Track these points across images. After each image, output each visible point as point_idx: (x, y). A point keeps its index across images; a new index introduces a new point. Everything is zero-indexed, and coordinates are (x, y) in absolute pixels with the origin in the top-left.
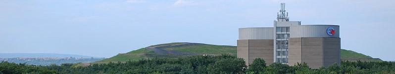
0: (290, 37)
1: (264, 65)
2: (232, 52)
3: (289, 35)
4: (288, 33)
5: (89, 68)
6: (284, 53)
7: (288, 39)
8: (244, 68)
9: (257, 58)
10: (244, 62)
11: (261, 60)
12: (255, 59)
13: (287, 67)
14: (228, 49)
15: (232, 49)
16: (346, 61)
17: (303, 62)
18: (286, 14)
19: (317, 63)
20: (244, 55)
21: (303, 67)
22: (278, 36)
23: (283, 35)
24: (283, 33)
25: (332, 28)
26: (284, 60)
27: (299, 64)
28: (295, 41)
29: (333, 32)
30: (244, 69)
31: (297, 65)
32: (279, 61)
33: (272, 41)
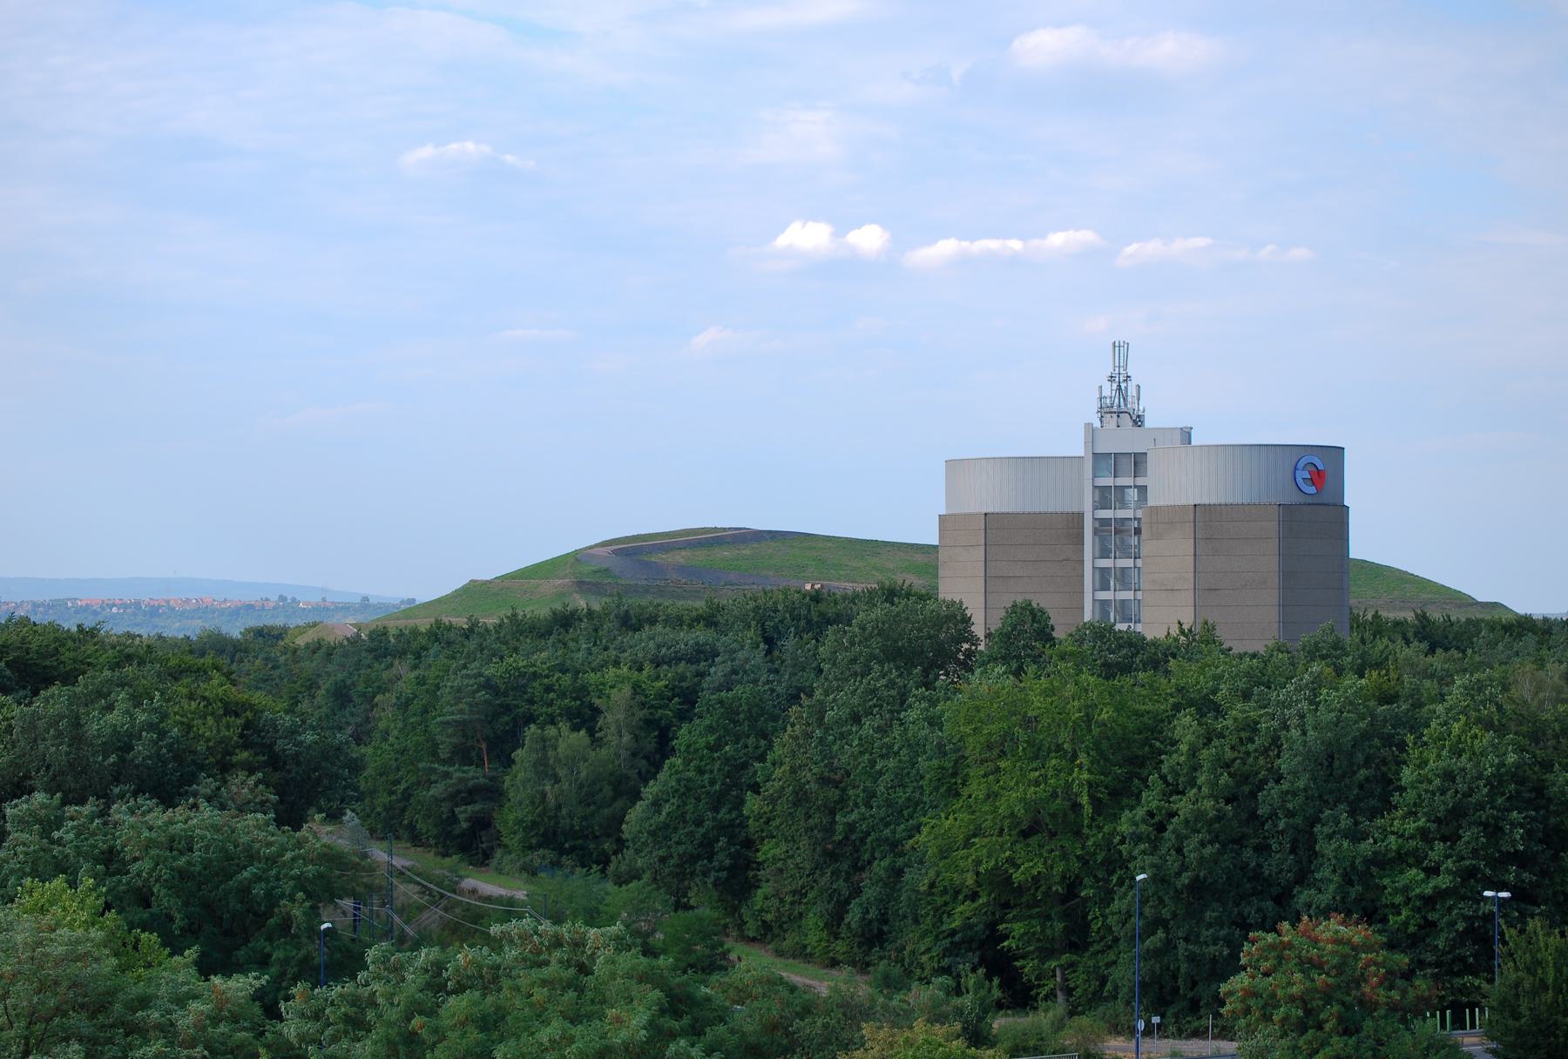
3: (1143, 490)
4: (1140, 481)
7: (1139, 514)
8: (966, 646)
9: (1019, 600)
10: (967, 621)
11: (1032, 611)
13: (1135, 644)
17: (1200, 620)
18: (1132, 391)
19: (1252, 628)
20: (963, 587)
21: (1199, 642)
22: (1105, 497)
24: (1121, 481)
28: (1168, 517)
29: (1317, 477)
30: (969, 654)
31: (1175, 631)
33: (1081, 516)
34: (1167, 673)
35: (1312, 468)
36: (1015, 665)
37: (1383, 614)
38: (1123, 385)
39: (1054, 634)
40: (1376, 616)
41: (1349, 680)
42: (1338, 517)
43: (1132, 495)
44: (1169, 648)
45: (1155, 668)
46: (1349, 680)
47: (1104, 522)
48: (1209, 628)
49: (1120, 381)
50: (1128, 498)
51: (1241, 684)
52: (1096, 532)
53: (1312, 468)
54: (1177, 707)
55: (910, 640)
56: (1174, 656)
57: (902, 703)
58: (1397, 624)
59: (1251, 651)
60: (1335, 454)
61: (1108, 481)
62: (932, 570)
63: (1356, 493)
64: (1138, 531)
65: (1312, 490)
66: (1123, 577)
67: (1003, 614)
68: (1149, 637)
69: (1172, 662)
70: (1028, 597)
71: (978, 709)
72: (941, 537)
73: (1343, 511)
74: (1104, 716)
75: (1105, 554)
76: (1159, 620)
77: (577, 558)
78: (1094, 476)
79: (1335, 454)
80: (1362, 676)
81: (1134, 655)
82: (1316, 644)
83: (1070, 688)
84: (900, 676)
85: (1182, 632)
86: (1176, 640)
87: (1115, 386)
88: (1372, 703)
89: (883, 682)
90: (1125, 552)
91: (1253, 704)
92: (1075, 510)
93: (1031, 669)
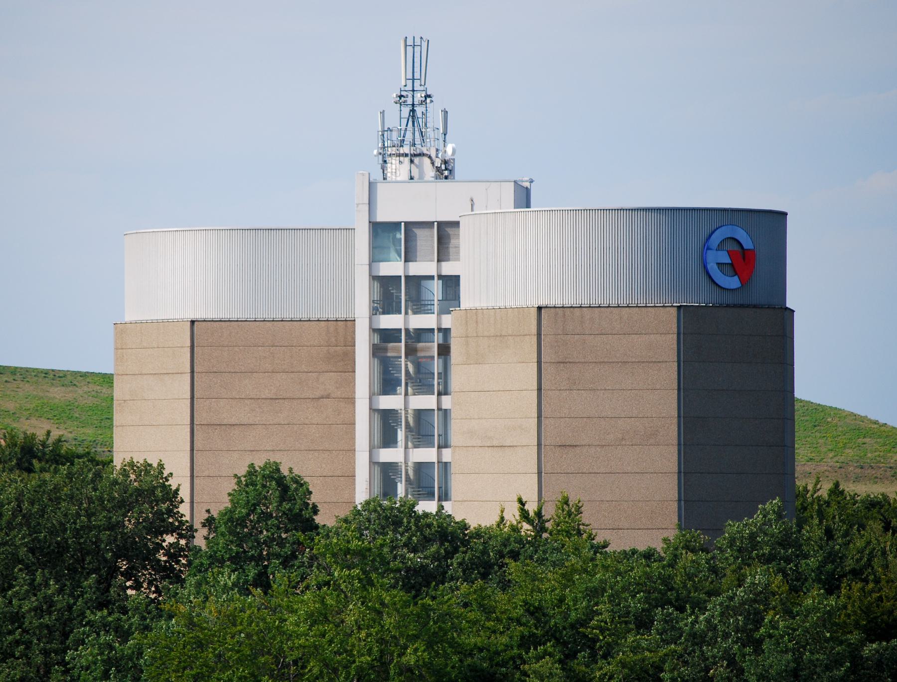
0: (467, 300)
1: (303, 520)
2: (63, 413)
3: (451, 283)
4: (448, 268)
5: (587, 552)
6: (422, 429)
7: (447, 321)
8: (170, 539)
9: (259, 463)
10: (172, 496)
11: (281, 482)
12: (242, 471)
13: (450, 536)
14: (409, 388)
15: (57, 394)
16: (824, 492)
17: (552, 496)
18: (435, 119)
19: (636, 507)
20: (150, 436)
21: (549, 536)
22: (387, 293)
23: (415, 282)
24: (417, 269)
25: (742, 236)
26: (424, 480)
27: (531, 508)
28: (495, 325)
29: (742, 261)
30: (174, 553)
31: (512, 515)
32: (388, 489)
33: (350, 323)
34: (505, 585)
35: (736, 248)
36: (252, 572)
37: (849, 488)
38: (419, 110)
39: (318, 519)
40: (836, 491)
41: (813, 597)
42: (772, 330)
43: (436, 289)
44: (506, 542)
45: (484, 576)
46: (813, 597)
47: (388, 335)
48: (570, 511)
49: (413, 105)
50: (426, 296)
51: (636, 604)
52: (377, 351)
53: (736, 248)
54: (527, 642)
55: (77, 533)
56: (515, 556)
57: (66, 635)
58: (872, 504)
59: (642, 548)
60: (776, 220)
61: (393, 267)
62: (103, 415)
63: (806, 287)
64: (444, 350)
65: (733, 282)
66: (422, 429)
67: (232, 485)
68: (473, 524)
69: (513, 566)
70: (275, 458)
71: (201, 645)
72: (119, 360)
73: (781, 320)
74: (410, 659)
75: (388, 385)
76: (486, 492)
77: (863, 419)
78: (374, 260)
79: (776, 220)
80: (830, 592)
81: (450, 555)
82: (752, 536)
83: (352, 614)
84: (61, 591)
85: (525, 515)
86: (515, 529)
87: (406, 111)
88: (854, 637)
89: (33, 602)
90: (421, 382)
91: (654, 636)
92: (342, 316)
93: (279, 578)
